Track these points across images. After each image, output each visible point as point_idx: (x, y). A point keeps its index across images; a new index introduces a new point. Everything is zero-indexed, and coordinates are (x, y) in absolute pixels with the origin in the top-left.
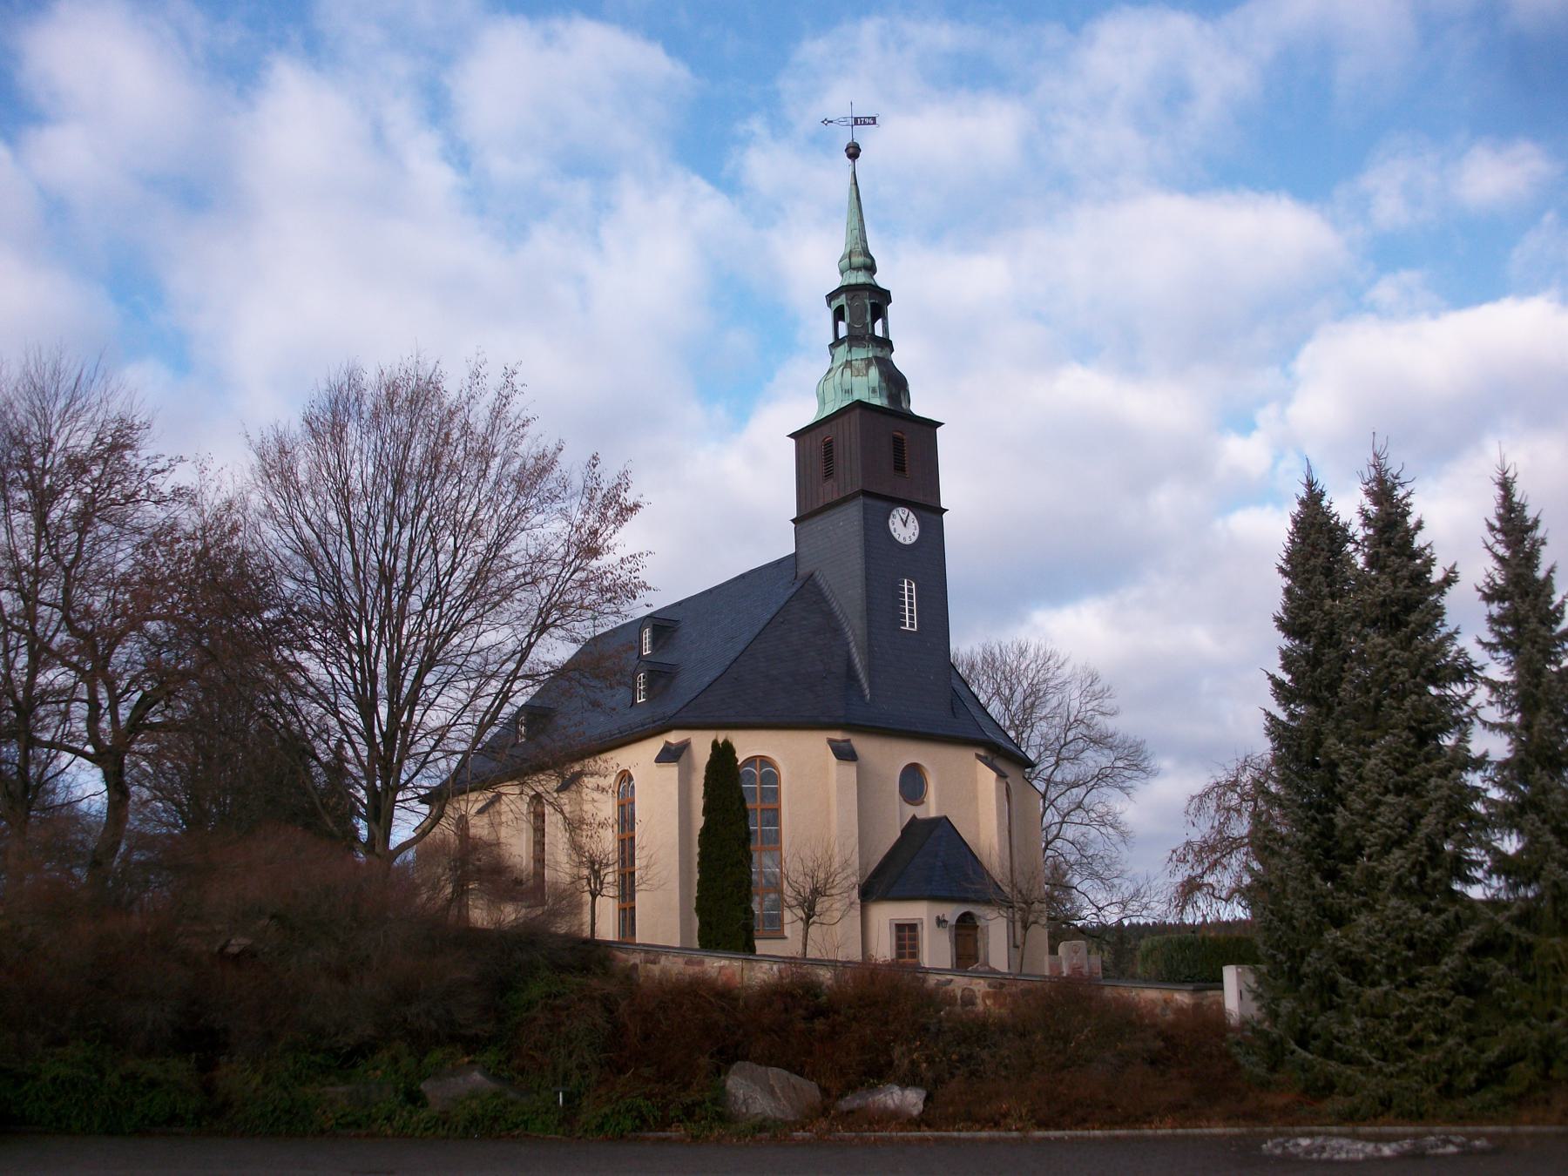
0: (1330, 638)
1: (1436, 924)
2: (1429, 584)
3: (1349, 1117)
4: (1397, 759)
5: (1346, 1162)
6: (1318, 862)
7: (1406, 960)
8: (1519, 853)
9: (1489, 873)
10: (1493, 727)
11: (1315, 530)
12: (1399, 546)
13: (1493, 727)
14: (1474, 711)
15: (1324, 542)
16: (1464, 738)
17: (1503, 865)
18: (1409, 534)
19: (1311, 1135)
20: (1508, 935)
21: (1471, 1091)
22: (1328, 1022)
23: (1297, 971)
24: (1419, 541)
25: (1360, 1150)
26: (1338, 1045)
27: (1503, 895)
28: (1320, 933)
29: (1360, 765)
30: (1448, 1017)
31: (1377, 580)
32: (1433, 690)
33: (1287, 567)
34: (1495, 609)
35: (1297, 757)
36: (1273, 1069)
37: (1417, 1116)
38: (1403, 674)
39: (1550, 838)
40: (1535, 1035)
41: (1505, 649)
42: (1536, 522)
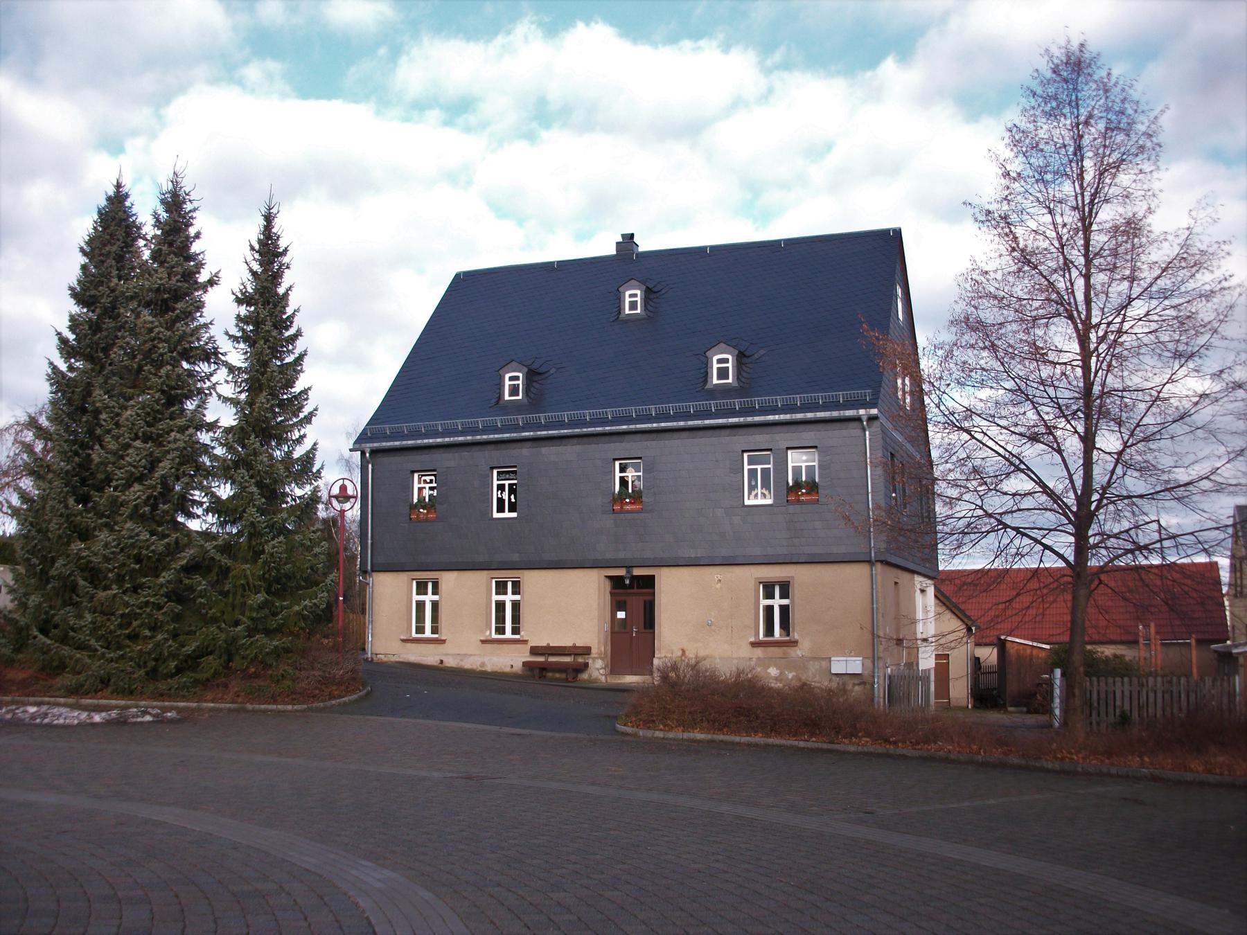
0: (111, 312)
1: (160, 546)
2: (196, 282)
3: (75, 691)
4: (148, 414)
5: (63, 727)
6: (74, 487)
7: (134, 570)
8: (229, 498)
9: (207, 511)
10: (226, 400)
11: (115, 217)
12: (178, 248)
13: (226, 400)
14: (214, 387)
15: (120, 234)
16: (202, 405)
17: (217, 506)
18: (188, 242)
19: (38, 704)
20: (213, 559)
21: (172, 676)
22: (66, 615)
23: (47, 573)
24: (195, 248)
25: (76, 717)
26: (72, 634)
27: (214, 529)
28: (68, 544)
29: (118, 415)
30: (161, 618)
31: (156, 271)
32: (185, 365)
33: (87, 249)
34: (243, 310)
35: (70, 402)
36: (18, 650)
37: (129, 693)
38: (163, 347)
39: (254, 489)
40: (223, 636)
41: (245, 342)
42: (286, 250)
